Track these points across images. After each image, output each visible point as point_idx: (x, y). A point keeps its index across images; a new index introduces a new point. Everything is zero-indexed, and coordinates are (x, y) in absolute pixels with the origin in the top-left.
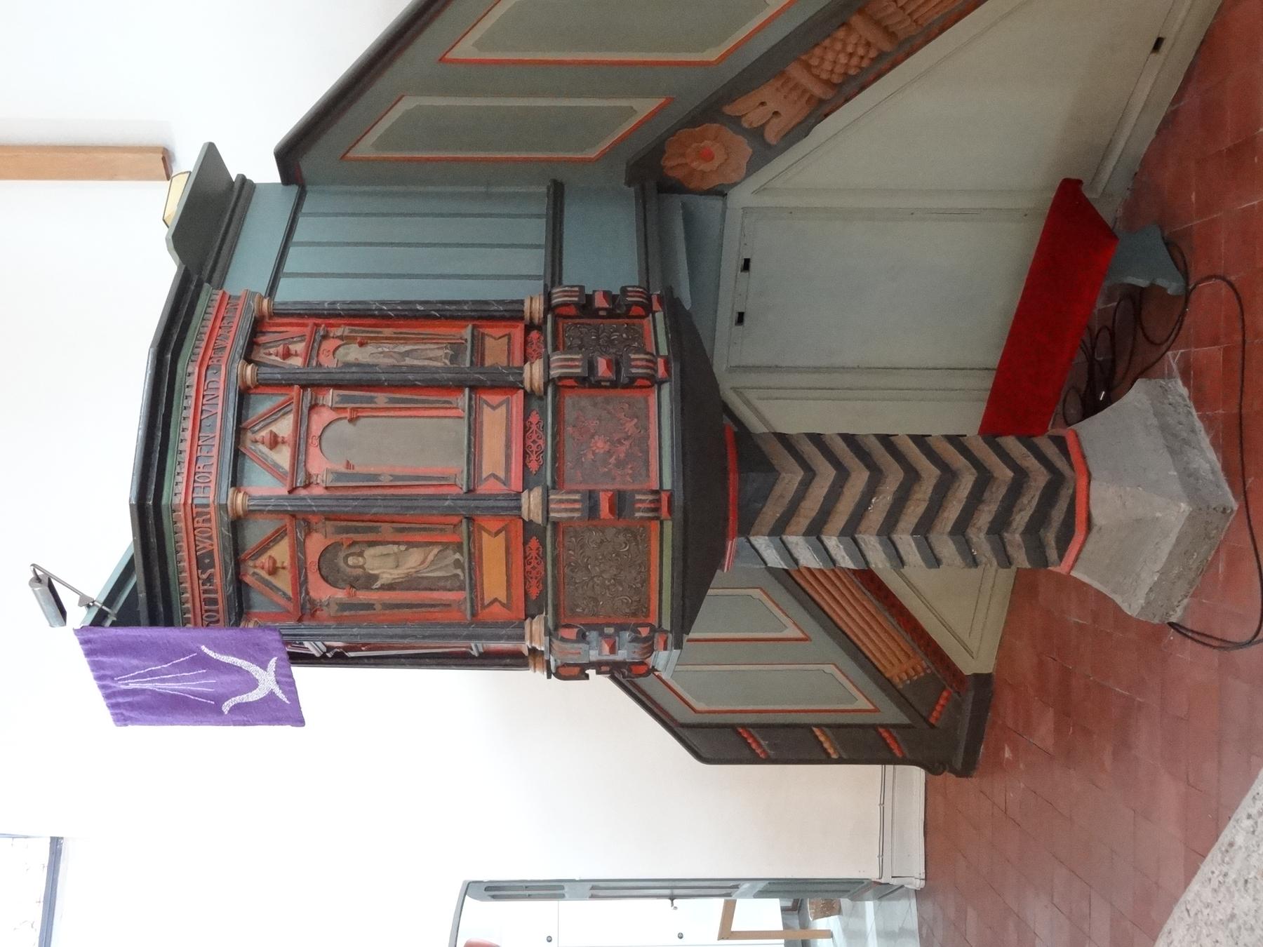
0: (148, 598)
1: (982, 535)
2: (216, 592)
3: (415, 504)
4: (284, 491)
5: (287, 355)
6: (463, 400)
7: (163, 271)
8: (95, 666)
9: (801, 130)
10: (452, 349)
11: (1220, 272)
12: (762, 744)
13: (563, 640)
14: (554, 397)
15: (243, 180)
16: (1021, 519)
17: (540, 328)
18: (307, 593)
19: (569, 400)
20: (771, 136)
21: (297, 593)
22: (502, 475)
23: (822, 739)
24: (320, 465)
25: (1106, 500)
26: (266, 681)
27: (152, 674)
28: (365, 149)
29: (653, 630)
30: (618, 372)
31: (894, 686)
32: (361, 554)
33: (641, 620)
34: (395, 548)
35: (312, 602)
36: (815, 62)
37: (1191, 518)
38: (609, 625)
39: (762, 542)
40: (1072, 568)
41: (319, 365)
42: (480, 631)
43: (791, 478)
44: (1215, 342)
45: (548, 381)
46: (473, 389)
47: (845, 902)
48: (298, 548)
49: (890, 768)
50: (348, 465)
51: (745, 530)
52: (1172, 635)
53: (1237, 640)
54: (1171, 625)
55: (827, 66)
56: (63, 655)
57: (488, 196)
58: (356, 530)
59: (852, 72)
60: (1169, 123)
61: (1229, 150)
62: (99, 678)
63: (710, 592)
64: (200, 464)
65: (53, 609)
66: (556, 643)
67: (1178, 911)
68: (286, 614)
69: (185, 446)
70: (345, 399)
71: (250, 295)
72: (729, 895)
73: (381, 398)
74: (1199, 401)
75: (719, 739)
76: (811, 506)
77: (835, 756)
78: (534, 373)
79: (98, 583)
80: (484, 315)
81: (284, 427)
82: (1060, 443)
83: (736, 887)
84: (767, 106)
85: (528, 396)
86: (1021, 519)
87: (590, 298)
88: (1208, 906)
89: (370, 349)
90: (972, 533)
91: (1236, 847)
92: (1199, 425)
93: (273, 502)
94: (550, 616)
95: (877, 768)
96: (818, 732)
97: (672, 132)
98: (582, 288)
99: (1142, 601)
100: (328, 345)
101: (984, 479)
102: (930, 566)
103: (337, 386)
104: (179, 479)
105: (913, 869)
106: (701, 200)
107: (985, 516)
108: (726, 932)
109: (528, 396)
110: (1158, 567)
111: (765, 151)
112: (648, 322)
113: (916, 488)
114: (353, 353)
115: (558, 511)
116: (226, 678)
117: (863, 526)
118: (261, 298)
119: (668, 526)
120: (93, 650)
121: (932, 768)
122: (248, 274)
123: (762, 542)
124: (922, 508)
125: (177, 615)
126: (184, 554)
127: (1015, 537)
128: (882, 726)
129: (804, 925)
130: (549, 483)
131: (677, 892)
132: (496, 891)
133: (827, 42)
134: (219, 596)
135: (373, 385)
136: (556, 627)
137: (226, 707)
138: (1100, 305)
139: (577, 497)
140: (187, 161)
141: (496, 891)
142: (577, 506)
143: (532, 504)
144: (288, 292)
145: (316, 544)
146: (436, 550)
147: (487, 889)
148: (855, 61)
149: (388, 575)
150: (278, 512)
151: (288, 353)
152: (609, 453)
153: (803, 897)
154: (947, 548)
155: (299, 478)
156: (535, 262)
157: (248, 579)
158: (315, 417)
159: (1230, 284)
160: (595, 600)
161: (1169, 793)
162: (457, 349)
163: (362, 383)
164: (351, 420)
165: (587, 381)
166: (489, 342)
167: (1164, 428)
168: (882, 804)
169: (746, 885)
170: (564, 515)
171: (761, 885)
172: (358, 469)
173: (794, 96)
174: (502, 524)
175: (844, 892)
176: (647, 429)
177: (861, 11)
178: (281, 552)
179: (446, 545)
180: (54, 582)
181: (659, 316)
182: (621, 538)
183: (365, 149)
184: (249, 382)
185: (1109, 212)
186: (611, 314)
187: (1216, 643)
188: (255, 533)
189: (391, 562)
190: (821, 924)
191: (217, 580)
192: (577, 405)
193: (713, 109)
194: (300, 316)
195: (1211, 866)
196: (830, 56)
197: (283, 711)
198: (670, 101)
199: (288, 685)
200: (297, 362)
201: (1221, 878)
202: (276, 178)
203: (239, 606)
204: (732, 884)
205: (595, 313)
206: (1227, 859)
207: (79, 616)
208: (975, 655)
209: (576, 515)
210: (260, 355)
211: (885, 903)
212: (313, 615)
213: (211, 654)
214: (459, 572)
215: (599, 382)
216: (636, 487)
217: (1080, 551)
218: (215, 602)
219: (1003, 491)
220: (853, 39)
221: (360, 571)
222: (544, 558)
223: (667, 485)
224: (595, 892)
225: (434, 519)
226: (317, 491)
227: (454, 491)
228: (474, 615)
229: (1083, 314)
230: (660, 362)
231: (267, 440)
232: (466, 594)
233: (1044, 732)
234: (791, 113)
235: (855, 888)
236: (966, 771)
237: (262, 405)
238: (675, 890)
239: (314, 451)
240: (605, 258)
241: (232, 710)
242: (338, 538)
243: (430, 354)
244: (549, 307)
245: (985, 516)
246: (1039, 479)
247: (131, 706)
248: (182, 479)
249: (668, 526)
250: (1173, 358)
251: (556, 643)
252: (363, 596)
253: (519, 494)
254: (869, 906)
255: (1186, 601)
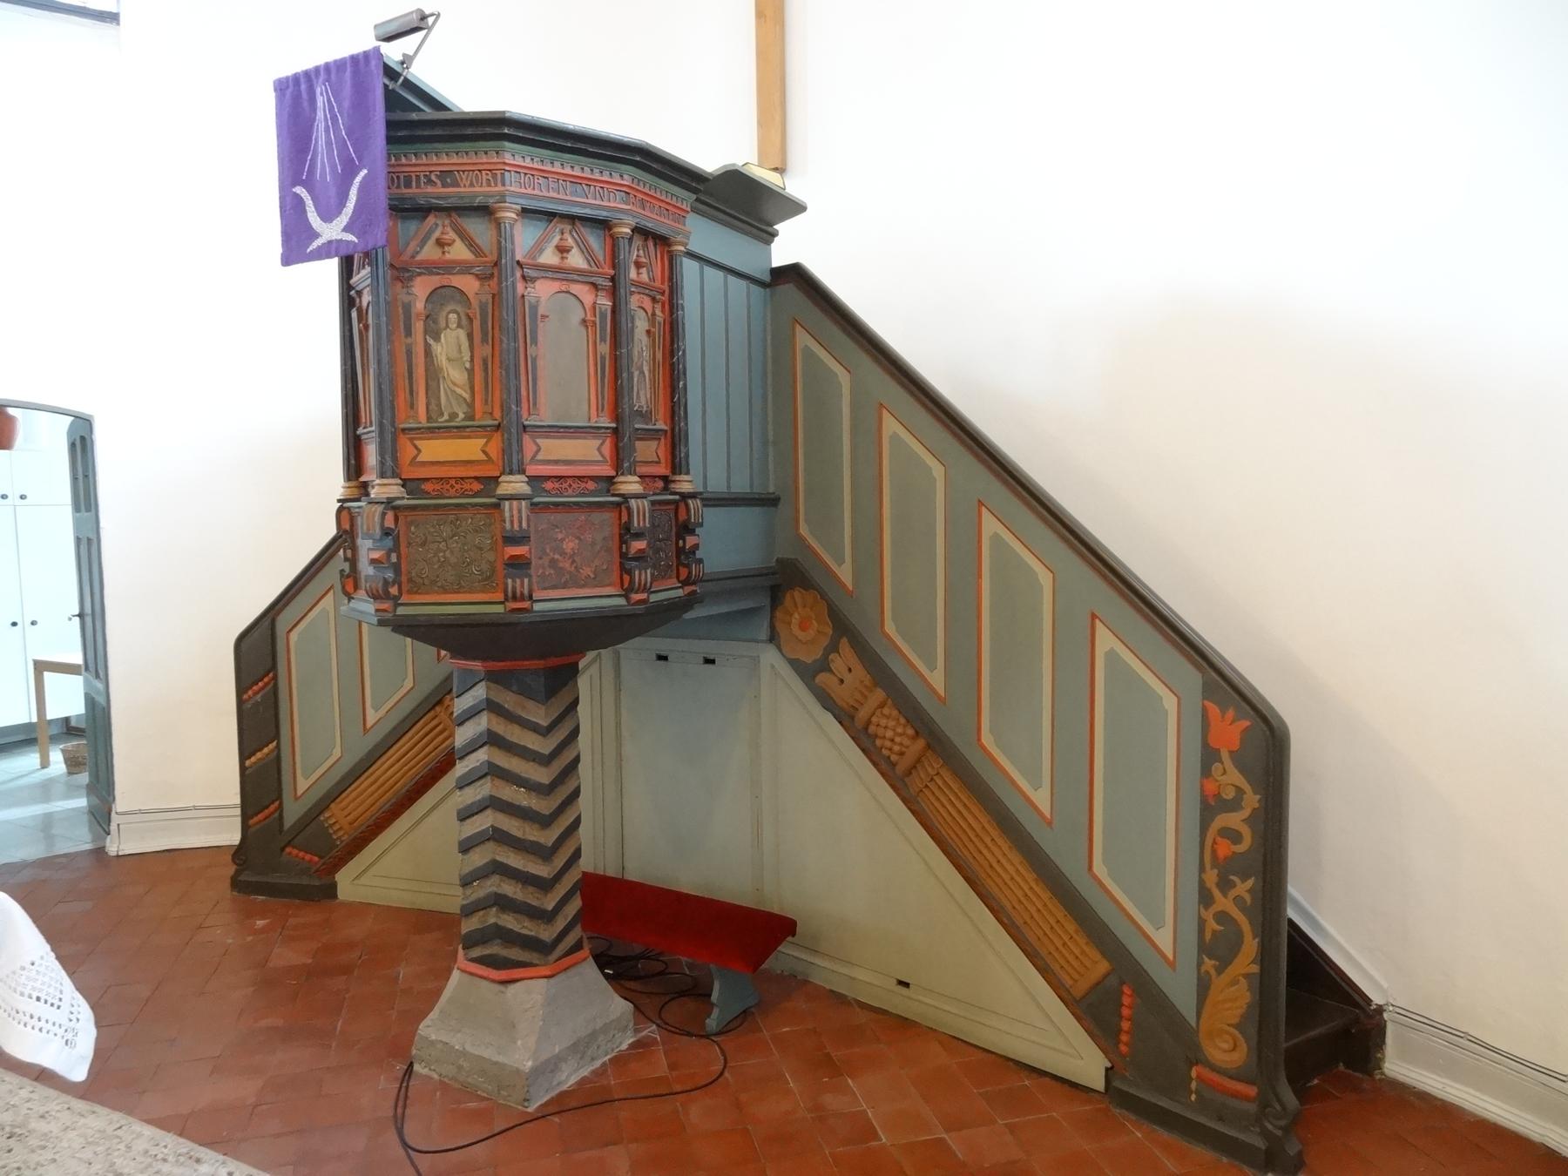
0: (414, 124)
1: (494, 889)
2: (418, 186)
3: (512, 377)
4: (518, 257)
5: (638, 265)
6: (606, 422)
7: (708, 160)
8: (340, 65)
9: (826, 701)
10: (646, 410)
11: (730, 1064)
12: (255, 695)
13: (384, 515)
14: (612, 503)
15: (774, 235)
16: (509, 921)
17: (666, 489)
18: (420, 274)
19: (608, 517)
20: (822, 678)
21: (421, 264)
22: (539, 457)
23: (266, 750)
24: (543, 291)
25: (529, 995)
26: (332, 231)
27: (334, 119)
28: (803, 339)
29: (396, 598)
30: (634, 559)
31: (321, 813)
32: (459, 326)
33: (405, 588)
34: (467, 356)
35: (410, 279)
36: (886, 711)
37: (518, 1071)
38: (399, 557)
39: (479, 692)
40: (463, 971)
41: (632, 293)
42: (389, 437)
43: (539, 715)
44: (673, 1066)
45: (626, 498)
46: (615, 431)
47: (84, 778)
48: (464, 268)
49: (238, 811)
50: (544, 317)
51: (493, 677)
52: (400, 1068)
53: (406, 1131)
54: (411, 1064)
55: (883, 722)
56: (347, 36)
57: (765, 443)
58: (484, 322)
59: (878, 742)
60: (839, 999)
61: (828, 1055)
62: (327, 66)
63: (409, 640)
64: (541, 181)
65: (392, 29)
66: (380, 508)
67: (117, 1117)
68: (398, 254)
69: (557, 168)
70: (603, 316)
71: (687, 235)
72: (87, 669)
73: (604, 348)
74: (619, 1061)
75: (260, 655)
76: (515, 734)
77: (248, 763)
78: (630, 485)
79: (424, 73)
80: (676, 439)
81: (576, 260)
82: (578, 947)
83: (97, 676)
84: (847, 671)
85: (610, 480)
86: (509, 921)
87: (692, 532)
88: (129, 1147)
89: (645, 339)
90: (495, 879)
91: (196, 1166)
92: (598, 1064)
93: (509, 246)
94: (405, 502)
95: (237, 800)
96: (272, 746)
97: (823, 596)
98: (701, 525)
99: (433, 1037)
100: (647, 303)
101: (544, 885)
102: (461, 843)
103: (614, 311)
104: (528, 159)
105: (123, 843)
106: (766, 624)
107: (510, 889)
108: (41, 667)
109: (610, 480)
110: (469, 1048)
111: (808, 673)
112: (674, 582)
113: (537, 826)
114: (641, 325)
115: (511, 509)
116: (332, 191)
117: (498, 782)
118: (685, 245)
119: (499, 609)
120: (359, 64)
121: (240, 853)
122: (704, 235)
123: (479, 692)
124: (519, 834)
125: (396, 149)
126: (455, 160)
127: (492, 917)
128: (281, 804)
129: (54, 739)
130: (536, 500)
131: (88, 620)
132: (81, 446)
133: (903, 721)
134: (414, 190)
135: (616, 343)
136: (395, 508)
137: (300, 190)
138: (684, 959)
139: (524, 525)
140: (793, 187)
141: (81, 446)
142: (516, 527)
143: (514, 484)
144: (689, 268)
145: (469, 284)
146: (466, 396)
147: (83, 438)
148: (888, 744)
149: (441, 350)
150: (500, 250)
151: (640, 268)
152: (563, 553)
153: (89, 740)
154: (479, 858)
155: (531, 271)
156: (717, 484)
157: (431, 220)
158: (586, 288)
159: (722, 1074)
160: (423, 544)
161: (244, 1089)
162: (646, 416)
163: (617, 333)
164: (584, 321)
165: (626, 532)
166: (654, 444)
167: (593, 1036)
168: (195, 808)
169: (100, 686)
170: (507, 515)
171: (101, 700)
172: (541, 325)
173: (859, 697)
174: (494, 455)
175: (95, 777)
176: (583, 586)
177: (929, 746)
178: (459, 251)
179: (471, 405)
180: (423, 33)
181: (680, 592)
182: (485, 567)
183: (803, 339)
184: (616, 230)
185: (773, 963)
186: (680, 551)
187: (400, 1110)
188: (478, 228)
189: (454, 354)
190: (57, 757)
191: (430, 189)
192: (605, 524)
193: (844, 629)
194: (671, 279)
195: (172, 1143)
196: (892, 723)
197: (297, 244)
198: (850, 594)
199: (323, 253)
200: (633, 274)
201: (160, 1156)
202: (775, 264)
203: (405, 209)
204: (102, 674)
205: (680, 536)
206: (182, 1159)
207: (393, 52)
208: (350, 883)
209: (508, 525)
210: (638, 242)
211: (85, 818)
212: (398, 279)
213: (358, 179)
214: (446, 417)
215: (626, 542)
216: (534, 579)
217: (481, 977)
218: (408, 185)
219: (535, 903)
220: (906, 742)
221: (443, 324)
222: (463, 496)
223: (537, 607)
224: (84, 542)
225: (497, 394)
226: (520, 287)
227: (525, 415)
228: (403, 430)
229: (686, 952)
230: (643, 596)
231: (564, 243)
232: (424, 423)
233: (287, 956)
234: (843, 695)
235: (102, 787)
236: (236, 884)
237: (594, 241)
238: (92, 618)
239: (556, 286)
240: (724, 543)
241: (297, 196)
242: (475, 303)
243: (643, 393)
244: (685, 497)
245: (510, 889)
246: (547, 933)
247: (297, 98)
248: (528, 163)
249: (499, 609)
250: (651, 1030)
251: (380, 508)
252: (419, 327)
253: (522, 472)
254: (82, 802)
255: (436, 1076)
